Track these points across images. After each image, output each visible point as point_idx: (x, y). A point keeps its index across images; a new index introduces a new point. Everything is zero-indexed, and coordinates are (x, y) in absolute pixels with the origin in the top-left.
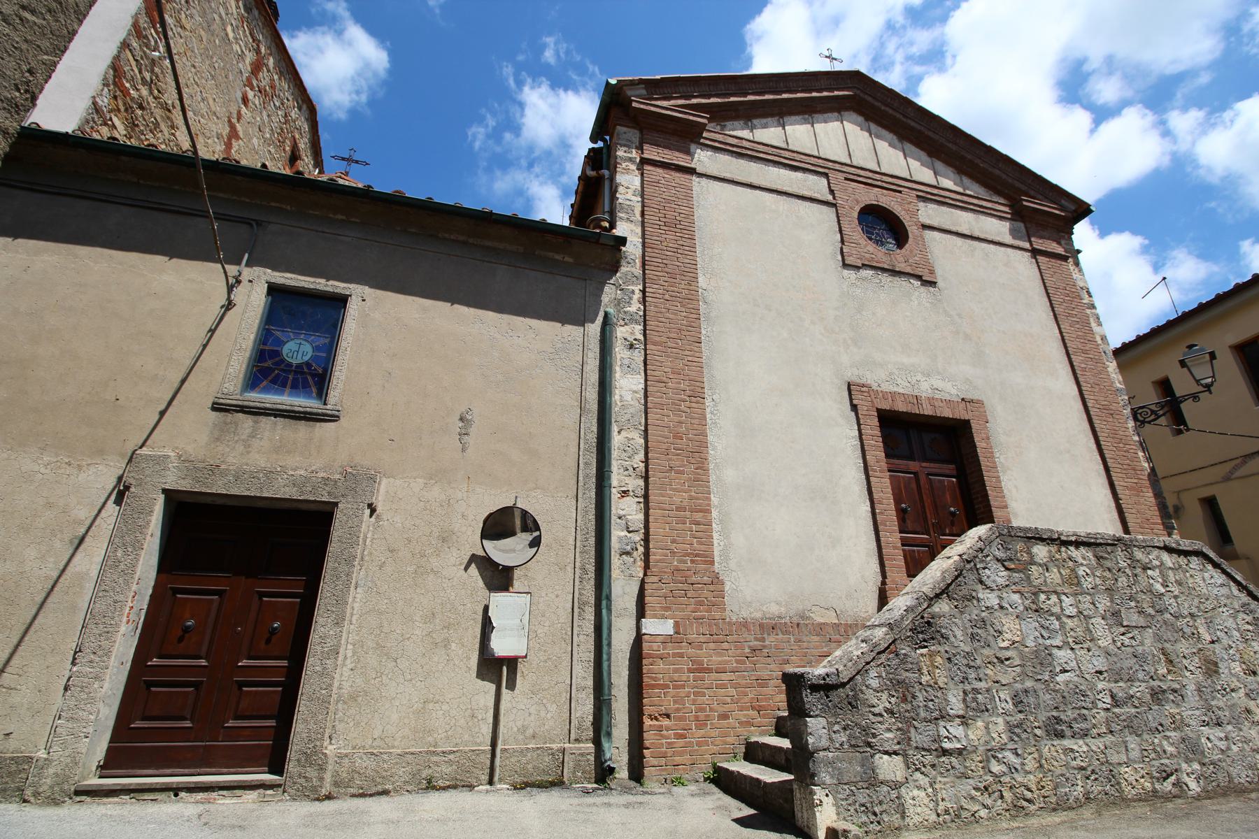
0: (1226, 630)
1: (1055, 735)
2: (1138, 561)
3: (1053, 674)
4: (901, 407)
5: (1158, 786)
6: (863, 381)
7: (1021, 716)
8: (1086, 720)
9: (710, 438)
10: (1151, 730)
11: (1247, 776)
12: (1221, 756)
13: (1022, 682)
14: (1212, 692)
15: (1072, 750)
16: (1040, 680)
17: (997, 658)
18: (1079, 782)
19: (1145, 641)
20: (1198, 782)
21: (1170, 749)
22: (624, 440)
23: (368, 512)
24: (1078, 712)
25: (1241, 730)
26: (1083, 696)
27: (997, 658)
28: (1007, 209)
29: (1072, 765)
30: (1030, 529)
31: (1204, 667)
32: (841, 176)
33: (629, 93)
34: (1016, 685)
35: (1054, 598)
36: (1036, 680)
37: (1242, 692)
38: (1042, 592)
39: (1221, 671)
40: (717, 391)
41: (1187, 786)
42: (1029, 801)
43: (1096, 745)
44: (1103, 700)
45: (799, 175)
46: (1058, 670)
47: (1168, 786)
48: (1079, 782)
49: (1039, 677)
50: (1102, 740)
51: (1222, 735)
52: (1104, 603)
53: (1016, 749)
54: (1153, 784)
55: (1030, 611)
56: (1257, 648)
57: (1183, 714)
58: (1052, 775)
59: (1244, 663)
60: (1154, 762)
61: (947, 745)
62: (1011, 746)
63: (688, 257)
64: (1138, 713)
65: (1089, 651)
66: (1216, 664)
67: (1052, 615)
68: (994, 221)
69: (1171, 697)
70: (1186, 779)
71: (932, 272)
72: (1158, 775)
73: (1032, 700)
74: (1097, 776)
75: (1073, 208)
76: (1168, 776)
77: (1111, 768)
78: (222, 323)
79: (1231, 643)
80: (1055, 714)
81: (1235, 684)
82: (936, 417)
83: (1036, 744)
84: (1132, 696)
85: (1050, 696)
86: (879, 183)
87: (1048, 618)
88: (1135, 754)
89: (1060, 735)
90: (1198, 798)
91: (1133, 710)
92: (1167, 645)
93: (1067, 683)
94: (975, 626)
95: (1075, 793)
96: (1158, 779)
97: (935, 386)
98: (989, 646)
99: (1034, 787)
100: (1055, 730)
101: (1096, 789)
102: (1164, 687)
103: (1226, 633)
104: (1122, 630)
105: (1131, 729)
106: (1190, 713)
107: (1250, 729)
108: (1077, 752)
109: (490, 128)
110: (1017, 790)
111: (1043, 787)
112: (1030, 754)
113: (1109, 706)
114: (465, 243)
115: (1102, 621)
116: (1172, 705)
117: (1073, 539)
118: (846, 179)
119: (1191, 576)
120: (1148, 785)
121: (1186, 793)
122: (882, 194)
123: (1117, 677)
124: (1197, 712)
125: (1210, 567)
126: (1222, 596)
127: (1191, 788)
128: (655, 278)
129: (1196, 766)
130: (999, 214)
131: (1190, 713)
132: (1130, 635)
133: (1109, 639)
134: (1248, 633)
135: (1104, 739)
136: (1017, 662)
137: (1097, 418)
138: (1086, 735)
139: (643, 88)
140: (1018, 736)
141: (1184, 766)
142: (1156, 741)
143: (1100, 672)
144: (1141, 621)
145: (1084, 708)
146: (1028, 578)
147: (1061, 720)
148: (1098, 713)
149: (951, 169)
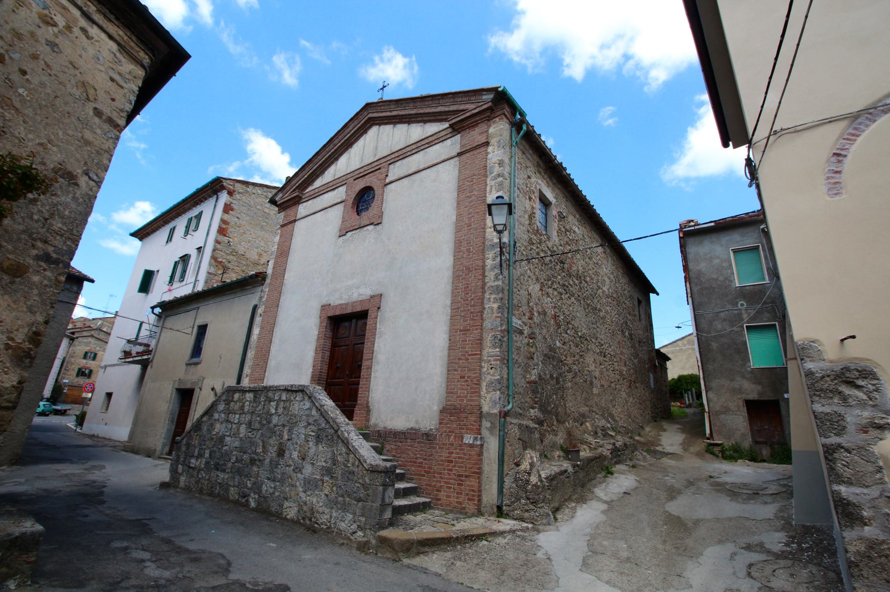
4: (338, 313)
5: (240, 499)
21: (249, 485)
22: (250, 354)
39: (285, 455)
66: (284, 451)
69: (258, 463)
81: (291, 462)
88: (236, 484)
89: (218, 470)
91: (241, 465)
96: (242, 497)
102: (256, 458)
109: (53, 281)
118: (355, 180)
124: (266, 472)
134: (311, 437)
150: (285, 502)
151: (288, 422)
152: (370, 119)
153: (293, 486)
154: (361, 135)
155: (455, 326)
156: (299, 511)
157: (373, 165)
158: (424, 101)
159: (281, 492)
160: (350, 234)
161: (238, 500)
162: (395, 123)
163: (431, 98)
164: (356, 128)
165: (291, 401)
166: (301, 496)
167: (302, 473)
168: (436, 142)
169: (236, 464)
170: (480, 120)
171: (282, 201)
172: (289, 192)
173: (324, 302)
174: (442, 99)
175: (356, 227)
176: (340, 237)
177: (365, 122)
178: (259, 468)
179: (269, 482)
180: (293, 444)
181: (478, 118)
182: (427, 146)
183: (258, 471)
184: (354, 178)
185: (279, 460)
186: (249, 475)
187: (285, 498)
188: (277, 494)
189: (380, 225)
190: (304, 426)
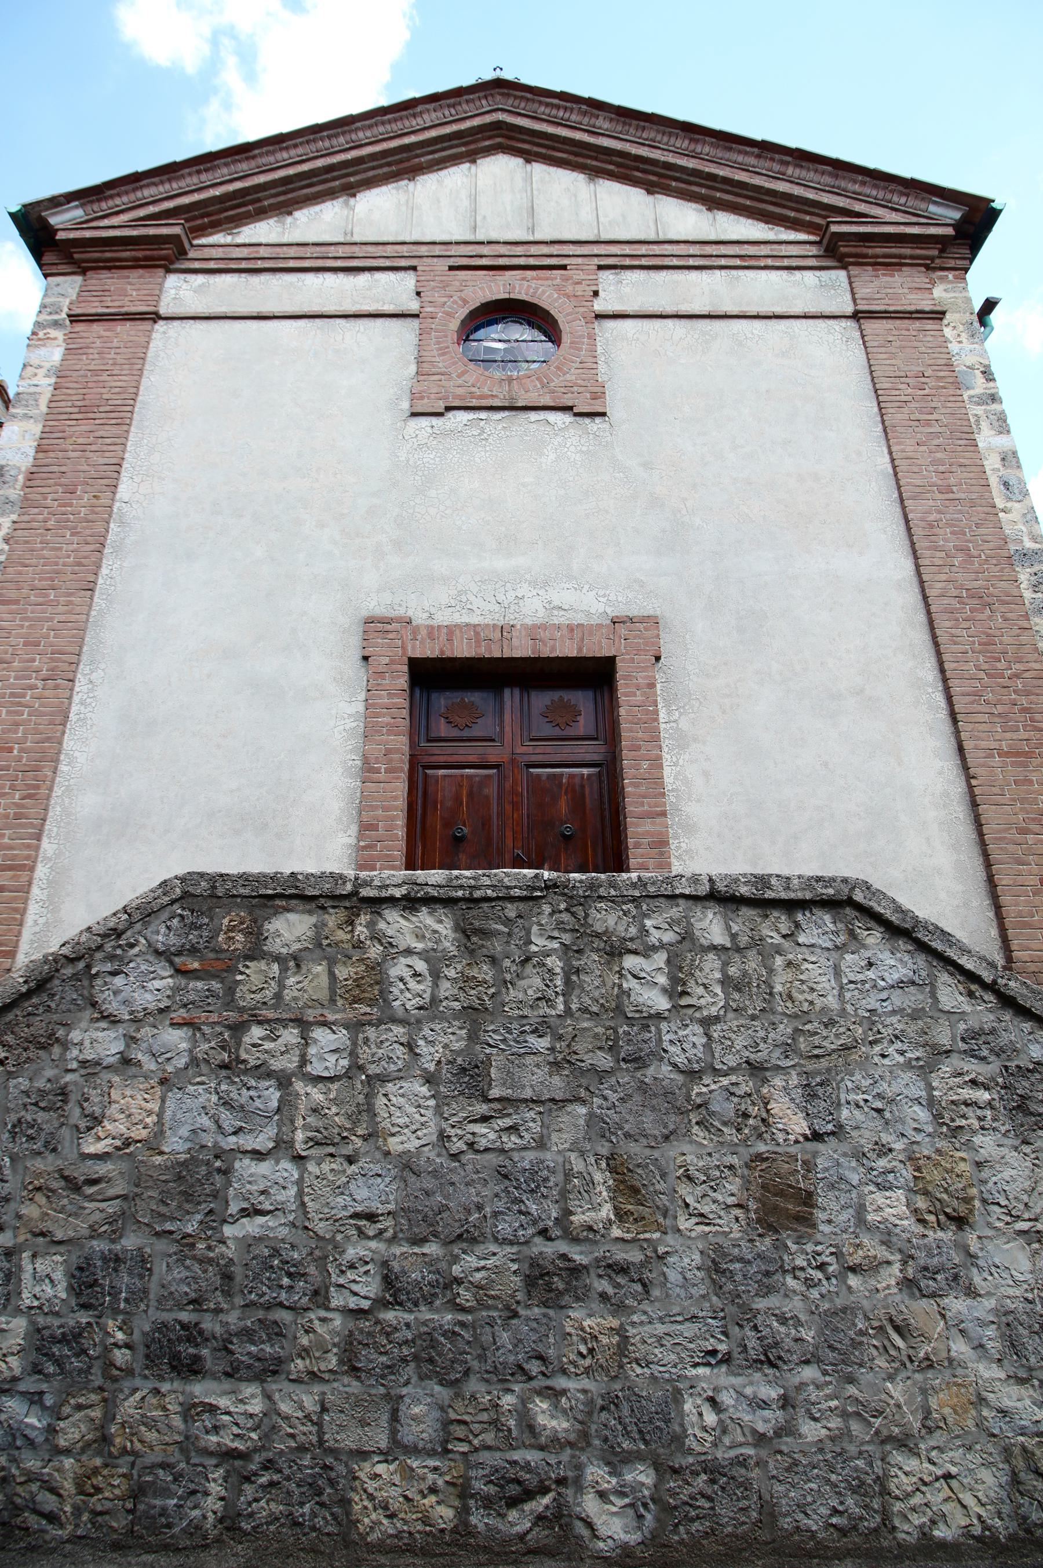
0: (878, 1104)
1: (173, 1368)
2: (598, 935)
3: (215, 1219)
5: (478, 1520)
6: (401, 612)
7: (84, 1318)
8: (280, 1334)
9: (68, 743)
10: (495, 1371)
11: (835, 1512)
12: (750, 1451)
13: (115, 1236)
14: (768, 1274)
15: (212, 1409)
16: (171, 1232)
17: (65, 1178)
18: (215, 1488)
19: (554, 1137)
20: (640, 1517)
24: (261, 1314)
26: (290, 1275)
27: (65, 1178)
28: (814, 250)
29: (202, 1444)
30: (274, 878)
31: (753, 1205)
32: (443, 265)
33: (53, 221)
34: (95, 1243)
35: (290, 1035)
36: (158, 1234)
38: (260, 1023)
39: (822, 1216)
40: (102, 666)
41: (590, 1525)
42: (52, 1518)
44: (355, 1287)
45: (364, 278)
46: (233, 1208)
48: (215, 1488)
49: (168, 1226)
50: (317, 1388)
53: (41, 1393)
54: (463, 1512)
55: (204, 1068)
56: (1039, 1144)
57: (631, 1331)
58: (133, 1464)
59: (926, 1193)
60: (484, 1456)
62: (29, 1385)
63: (107, 454)
64: (462, 1324)
65: (351, 1163)
67: (269, 1075)
68: (774, 276)
69: (603, 1285)
70: (590, 1505)
71: (598, 395)
72: (492, 1489)
73: (124, 1280)
74: (276, 1477)
75: (957, 215)
76: (529, 1495)
77: (329, 1460)
79: (885, 1138)
81: (872, 1247)
83: (108, 1385)
84: (459, 1281)
85: (185, 1273)
86: (522, 261)
87: (253, 1083)
89: (192, 1369)
93: (248, 1243)
94: (36, 1104)
95: (196, 1513)
97: (556, 603)
98: (54, 1150)
99: (68, 1486)
100: (175, 1356)
101: (267, 1508)
103: (879, 1111)
104: (482, 1109)
105: (426, 1368)
106: (660, 1329)
107: (891, 1378)
108: (228, 1413)
110: (19, 1489)
111: (98, 1490)
112: (79, 1407)
113: (365, 1304)
115: (424, 1090)
116: (596, 1305)
117: (398, 893)
118: (451, 268)
119: (789, 964)
120: (445, 1514)
121: (584, 1548)
122: (523, 279)
123: (422, 1230)
124: (689, 1329)
125: (874, 938)
126: (894, 1012)
127: (603, 1531)
128: (39, 497)
129: (642, 1476)
130: (786, 262)
131: (660, 1329)
132: (508, 1122)
133: (430, 1133)
134: (969, 1111)
135: (325, 1388)
136: (119, 1188)
137: (946, 616)
138: (275, 1373)
139: (76, 207)
140: (59, 1362)
141: (596, 1472)
142: (508, 1401)
143: (371, 1217)
144: (557, 1085)
145: (281, 1305)
146: (231, 990)
147: (201, 1332)
148: (323, 1320)
149: (694, 205)
150: (898, 1457)
151: (788, 1049)
152: (498, 125)
153: (928, 1364)
154: (455, 160)
155: (979, 739)
156: (1015, 1481)
157: (534, 250)
158: (730, 149)
159: (845, 1415)
160: (463, 417)
161: (463, 1529)
162: (595, 173)
163: (756, 150)
164: (447, 130)
165: (767, 953)
166: (1007, 1403)
167: (971, 1292)
168: (770, 262)
169: (390, 1316)
170: (912, 257)
171: (72, 235)
172: (142, 212)
173: (376, 605)
174: (796, 166)
175: (497, 403)
176: (414, 415)
177: (482, 128)
178: (619, 1308)
179: (722, 1376)
180: (860, 1155)
181: (908, 252)
182: (738, 262)
183: (620, 1331)
184: (452, 262)
185: (780, 1246)
186: (534, 1367)
187: (890, 1439)
188: (811, 1431)
189: (598, 420)
190: (908, 1065)
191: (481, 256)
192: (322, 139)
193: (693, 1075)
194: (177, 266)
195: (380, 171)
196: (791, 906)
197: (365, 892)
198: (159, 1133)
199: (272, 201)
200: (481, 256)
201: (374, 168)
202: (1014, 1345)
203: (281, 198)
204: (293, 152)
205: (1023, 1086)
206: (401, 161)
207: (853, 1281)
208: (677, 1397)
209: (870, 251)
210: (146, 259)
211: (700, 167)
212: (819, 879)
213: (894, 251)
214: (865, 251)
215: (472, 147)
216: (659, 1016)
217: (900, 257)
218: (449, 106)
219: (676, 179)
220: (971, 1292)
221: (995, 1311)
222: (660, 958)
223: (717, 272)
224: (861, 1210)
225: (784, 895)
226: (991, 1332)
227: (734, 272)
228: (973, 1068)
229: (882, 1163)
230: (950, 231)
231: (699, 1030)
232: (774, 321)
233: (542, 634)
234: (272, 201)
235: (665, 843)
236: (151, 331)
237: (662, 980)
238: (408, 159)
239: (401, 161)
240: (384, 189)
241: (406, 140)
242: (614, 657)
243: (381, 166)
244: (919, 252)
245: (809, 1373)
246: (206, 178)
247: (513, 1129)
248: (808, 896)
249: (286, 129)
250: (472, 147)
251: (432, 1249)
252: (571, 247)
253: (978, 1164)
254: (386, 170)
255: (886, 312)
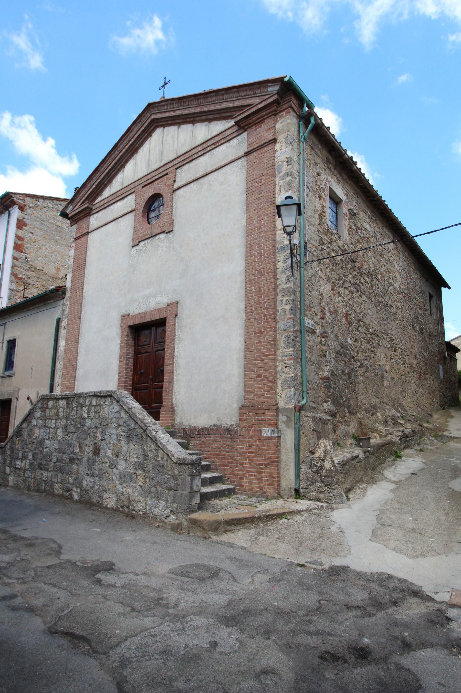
4: (138, 322)
5: (64, 493)
22: (59, 365)
23: (16, 400)
25: (101, 480)
37: (108, 464)
39: (101, 453)
43: (50, 474)
47: (68, 494)
51: (92, 481)
52: (63, 422)
54: (63, 492)
61: (17, 466)
66: (99, 450)
69: (76, 462)
70: (74, 493)
78: (391, 204)
80: (41, 462)
81: (106, 460)
82: (135, 325)
88: (59, 480)
90: (77, 502)
92: (81, 441)
101: (48, 488)
102: (75, 457)
104: (66, 433)
114: (33, 308)
117: (60, 397)
118: (143, 187)
120: (61, 492)
124: (85, 469)
129: (79, 490)
134: (122, 437)
136: (36, 444)
141: (75, 489)
142: (67, 477)
150: (105, 493)
154: (146, 139)
157: (160, 170)
161: (63, 494)
164: (140, 132)
166: (118, 488)
167: (117, 469)
168: (222, 141)
170: (267, 114)
172: (79, 204)
173: (124, 312)
176: (133, 247)
177: (149, 124)
182: (213, 146)
183: (78, 469)
184: (142, 185)
187: (104, 490)
188: (96, 487)
189: (171, 233)
191: (148, 179)
192: (112, 155)
193: (89, 428)
194: (92, 213)
195: (128, 156)
196: (105, 397)
197: (57, 397)
198: (39, 436)
199: (107, 181)
200: (148, 179)
201: (126, 156)
202: (120, 478)
203: (108, 179)
204: (108, 163)
205: (129, 432)
206: (132, 149)
207: (103, 465)
208: (83, 479)
209: (251, 121)
210: (85, 215)
211: (203, 110)
212: (108, 391)
213: (259, 116)
214: (249, 122)
215: (148, 132)
216: (85, 418)
217: (262, 117)
218: (139, 122)
219: (197, 117)
220: (117, 469)
221: (119, 472)
222: (87, 407)
223: (208, 154)
224: (106, 453)
225: (103, 395)
226: (118, 476)
227: (212, 151)
228: (123, 428)
229: (109, 445)
230: (276, 96)
231: (90, 420)
232: (221, 169)
233: (153, 313)
234: (107, 181)
235: (173, 372)
236: (87, 238)
237: (87, 412)
238: (134, 147)
239: (132, 149)
240: (129, 163)
241: (131, 142)
242: (165, 318)
243: (128, 154)
244: (268, 111)
245: (97, 478)
246: (92, 183)
247: (69, 437)
248: (106, 395)
249: (103, 158)
250: (148, 132)
251: (61, 454)
252: (169, 164)
253: (121, 447)
254: (129, 155)
255: (254, 149)
